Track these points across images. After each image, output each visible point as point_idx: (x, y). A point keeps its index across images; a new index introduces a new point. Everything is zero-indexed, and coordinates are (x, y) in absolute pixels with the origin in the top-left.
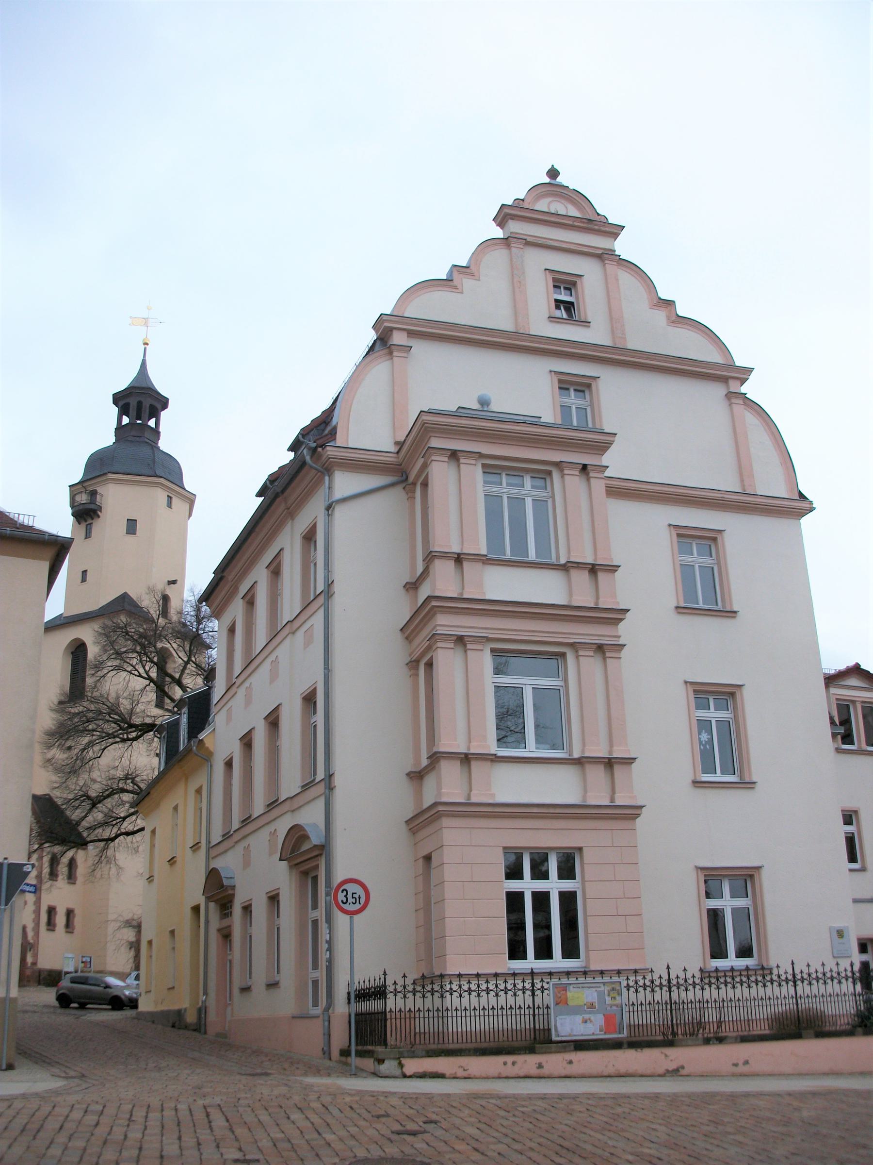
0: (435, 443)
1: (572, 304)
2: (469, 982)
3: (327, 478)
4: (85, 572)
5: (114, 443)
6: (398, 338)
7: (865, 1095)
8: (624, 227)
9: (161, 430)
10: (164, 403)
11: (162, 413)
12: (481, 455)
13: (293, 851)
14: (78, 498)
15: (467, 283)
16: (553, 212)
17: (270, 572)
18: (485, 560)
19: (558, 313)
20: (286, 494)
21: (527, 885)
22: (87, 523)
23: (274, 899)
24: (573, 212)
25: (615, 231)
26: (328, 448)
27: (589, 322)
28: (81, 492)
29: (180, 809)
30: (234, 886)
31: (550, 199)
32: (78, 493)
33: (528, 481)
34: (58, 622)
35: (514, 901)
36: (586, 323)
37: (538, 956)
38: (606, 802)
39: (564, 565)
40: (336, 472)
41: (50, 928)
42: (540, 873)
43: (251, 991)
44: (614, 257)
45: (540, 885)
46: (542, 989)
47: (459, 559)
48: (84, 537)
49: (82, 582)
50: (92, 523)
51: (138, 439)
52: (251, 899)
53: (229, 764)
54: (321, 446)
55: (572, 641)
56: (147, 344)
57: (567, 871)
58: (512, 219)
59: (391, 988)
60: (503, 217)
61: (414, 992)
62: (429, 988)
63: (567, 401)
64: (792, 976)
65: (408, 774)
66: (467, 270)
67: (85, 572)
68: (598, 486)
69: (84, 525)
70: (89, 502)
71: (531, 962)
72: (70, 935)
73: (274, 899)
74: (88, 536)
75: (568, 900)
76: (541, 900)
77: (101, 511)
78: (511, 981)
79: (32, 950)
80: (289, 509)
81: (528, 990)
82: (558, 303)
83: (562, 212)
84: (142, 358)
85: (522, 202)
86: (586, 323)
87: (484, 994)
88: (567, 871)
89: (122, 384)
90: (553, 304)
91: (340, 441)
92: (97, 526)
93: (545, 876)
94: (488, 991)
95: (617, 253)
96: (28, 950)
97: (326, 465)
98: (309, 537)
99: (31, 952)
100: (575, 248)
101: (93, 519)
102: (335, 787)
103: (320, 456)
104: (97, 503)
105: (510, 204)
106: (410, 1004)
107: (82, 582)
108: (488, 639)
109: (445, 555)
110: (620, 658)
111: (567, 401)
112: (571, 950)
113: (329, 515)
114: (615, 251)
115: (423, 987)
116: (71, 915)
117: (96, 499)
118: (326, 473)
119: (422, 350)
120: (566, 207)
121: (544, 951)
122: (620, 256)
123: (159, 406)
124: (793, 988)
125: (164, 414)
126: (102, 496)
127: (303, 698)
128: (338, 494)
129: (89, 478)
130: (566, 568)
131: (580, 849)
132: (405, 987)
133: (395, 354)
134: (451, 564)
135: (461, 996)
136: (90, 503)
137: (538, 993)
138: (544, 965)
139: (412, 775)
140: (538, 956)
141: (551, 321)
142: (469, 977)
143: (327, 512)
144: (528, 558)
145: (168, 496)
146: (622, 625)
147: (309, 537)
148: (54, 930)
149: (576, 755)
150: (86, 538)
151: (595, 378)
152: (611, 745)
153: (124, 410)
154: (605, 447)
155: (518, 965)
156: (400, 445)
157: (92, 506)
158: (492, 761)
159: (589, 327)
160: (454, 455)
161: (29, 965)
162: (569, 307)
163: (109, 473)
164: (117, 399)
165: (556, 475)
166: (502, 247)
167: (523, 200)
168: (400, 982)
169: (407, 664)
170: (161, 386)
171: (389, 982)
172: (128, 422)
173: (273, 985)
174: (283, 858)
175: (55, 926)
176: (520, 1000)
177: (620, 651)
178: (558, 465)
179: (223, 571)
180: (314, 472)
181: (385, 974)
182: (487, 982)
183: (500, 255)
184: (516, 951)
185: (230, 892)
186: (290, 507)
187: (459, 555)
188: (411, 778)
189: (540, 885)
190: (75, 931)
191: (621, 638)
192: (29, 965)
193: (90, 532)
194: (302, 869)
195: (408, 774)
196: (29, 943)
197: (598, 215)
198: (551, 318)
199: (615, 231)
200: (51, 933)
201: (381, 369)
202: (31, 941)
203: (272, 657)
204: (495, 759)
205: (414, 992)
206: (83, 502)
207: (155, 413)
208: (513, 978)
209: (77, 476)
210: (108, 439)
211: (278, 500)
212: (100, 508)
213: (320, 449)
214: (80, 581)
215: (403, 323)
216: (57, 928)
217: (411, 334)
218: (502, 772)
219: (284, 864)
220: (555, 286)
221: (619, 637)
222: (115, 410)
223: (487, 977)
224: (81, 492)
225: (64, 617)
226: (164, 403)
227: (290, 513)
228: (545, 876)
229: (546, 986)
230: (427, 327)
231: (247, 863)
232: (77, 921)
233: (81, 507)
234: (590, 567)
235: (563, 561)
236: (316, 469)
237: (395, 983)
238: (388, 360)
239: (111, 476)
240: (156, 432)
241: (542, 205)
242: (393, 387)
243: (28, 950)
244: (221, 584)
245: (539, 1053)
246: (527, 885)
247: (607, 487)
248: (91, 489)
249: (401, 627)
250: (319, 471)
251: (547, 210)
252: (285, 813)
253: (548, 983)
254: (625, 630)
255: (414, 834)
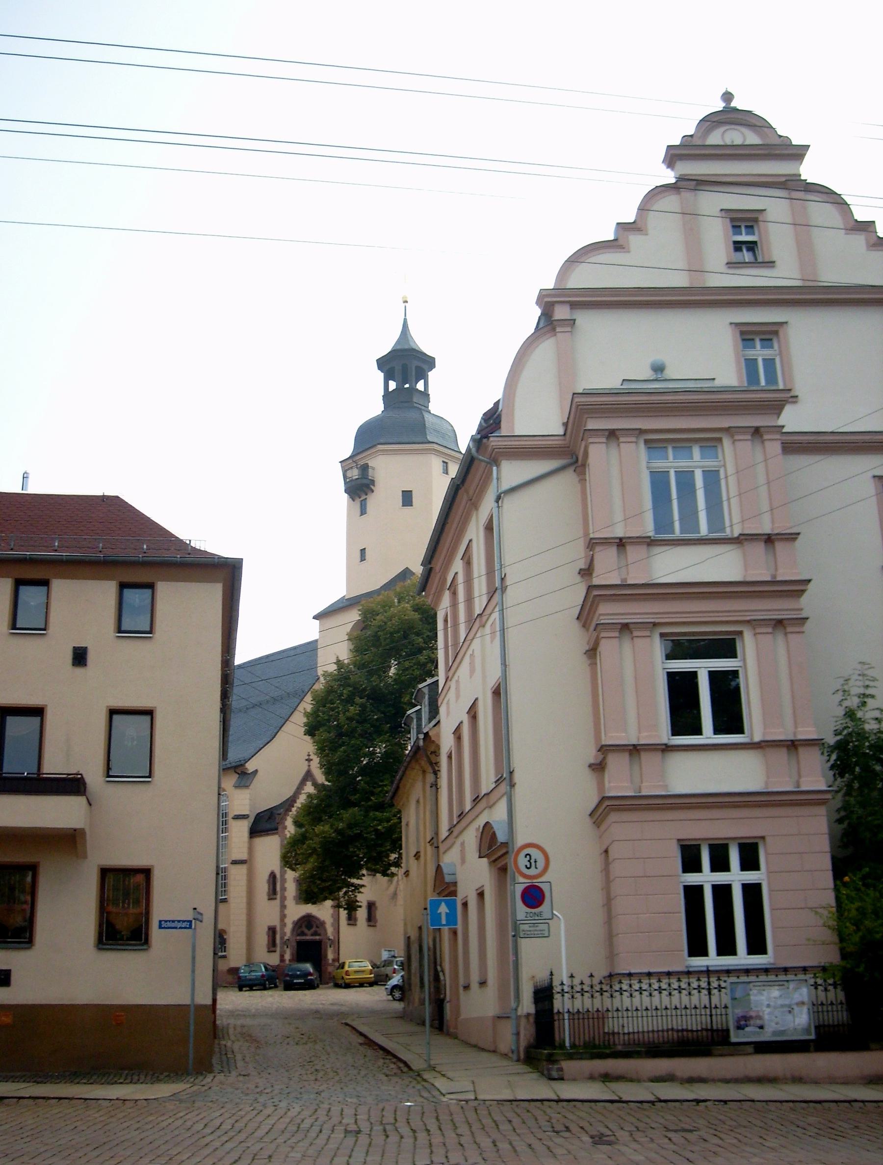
0: (592, 424)
1: (755, 243)
2: (640, 982)
3: (495, 468)
4: (363, 551)
5: (382, 412)
6: (561, 313)
7: (6, 1079)
8: (809, 146)
9: (431, 391)
10: (430, 363)
11: (429, 373)
12: (641, 432)
13: (490, 847)
14: (349, 474)
15: (634, 240)
16: (729, 144)
17: (463, 563)
18: (651, 542)
19: (737, 257)
20: (466, 484)
21: (707, 878)
22: (361, 499)
23: (481, 895)
24: (752, 138)
25: (798, 153)
26: (491, 439)
27: (774, 262)
28: (352, 468)
29: (421, 801)
30: (456, 883)
31: (722, 129)
32: (348, 469)
33: (696, 452)
34: (341, 605)
35: (693, 894)
36: (770, 264)
37: (720, 952)
38: (790, 788)
39: (737, 538)
40: (502, 461)
41: (351, 922)
42: (720, 864)
43: (470, 989)
44: (799, 183)
45: (721, 878)
46: (720, 988)
47: (621, 543)
48: (359, 513)
49: (362, 560)
50: (366, 499)
51: (406, 405)
52: (467, 897)
53: (450, 757)
54: (485, 438)
55: (748, 618)
56: (407, 302)
57: (750, 862)
58: (681, 160)
59: (557, 989)
60: (673, 156)
61: (602, 991)
62: (617, 987)
63: (751, 353)
64: (706, 984)
65: (590, 766)
66: (633, 226)
67: (363, 551)
68: (774, 448)
69: (358, 501)
70: (360, 477)
71: (713, 960)
72: (372, 928)
73: (481, 895)
74: (363, 513)
75: (752, 892)
76: (722, 893)
77: (374, 486)
78: (645, 981)
79: (332, 946)
80: (471, 500)
81: (703, 989)
82: (738, 246)
83: (738, 141)
84: (404, 317)
85: (690, 138)
86: (770, 264)
87: (656, 993)
88: (750, 862)
89: (385, 349)
90: (731, 246)
91: (504, 431)
92: (373, 501)
93: (726, 868)
94: (660, 990)
95: (802, 178)
96: (329, 946)
97: (493, 455)
98: (489, 528)
99: (332, 948)
100: (758, 180)
101: (366, 495)
102: (515, 784)
103: (487, 447)
104: (370, 478)
105: (678, 143)
106: (597, 1003)
107: (362, 560)
108: (655, 625)
109: (605, 542)
110: (803, 632)
111: (751, 353)
112: (757, 945)
113: (498, 507)
114: (800, 175)
115: (611, 987)
116: (373, 908)
117: (368, 472)
118: (493, 463)
119: (587, 321)
120: (743, 134)
121: (726, 947)
122: (806, 180)
123: (425, 367)
124: (707, 997)
125: (431, 375)
126: (373, 469)
127: (493, 692)
128: (505, 485)
129: (359, 451)
130: (740, 540)
131: (763, 838)
132: (592, 987)
133: (558, 329)
134: (613, 551)
135: (592, 996)
136: (361, 478)
137: (715, 992)
138: (727, 961)
139: (594, 767)
140: (720, 952)
141: (729, 267)
142: (640, 976)
143: (496, 505)
144: (699, 533)
145: (443, 462)
146: (806, 595)
147: (489, 528)
148: (356, 925)
149: (757, 738)
150: (362, 514)
151: (781, 324)
152: (796, 726)
153: (389, 376)
154: (781, 405)
155: (699, 962)
156: (566, 425)
157: (365, 481)
158: (663, 751)
159: (773, 267)
160: (612, 434)
161: (330, 961)
162: (752, 246)
163: (378, 444)
164: (384, 364)
165: (727, 442)
166: (667, 194)
167: (691, 136)
168: (587, 981)
169: (585, 653)
170: (424, 343)
171: (556, 983)
172: (395, 387)
173: (483, 983)
174: (482, 855)
175: (356, 920)
176: (695, 999)
177: (803, 624)
178: (727, 430)
179: (430, 563)
180: (483, 464)
181: (552, 974)
182: (659, 981)
183: (671, 202)
184: (697, 947)
185: (452, 889)
186: (473, 497)
187: (621, 539)
188: (593, 770)
189: (721, 878)
190: (378, 924)
191: (803, 611)
192: (330, 961)
193: (365, 509)
194: (500, 865)
195: (590, 766)
196: (329, 939)
197: (780, 136)
198: (730, 264)
199: (798, 153)
200: (351, 928)
201: (547, 347)
202: (331, 937)
203: (470, 652)
204: (667, 749)
205: (602, 991)
206: (354, 478)
207: (422, 375)
208: (628, 978)
209: (347, 449)
210: (376, 408)
211: (460, 492)
212: (373, 482)
213: (485, 440)
214: (360, 560)
215: (565, 296)
216: (358, 923)
217: (574, 305)
218: (677, 761)
219: (485, 860)
220: (734, 227)
221: (802, 609)
222: (381, 376)
223: (660, 976)
224: (352, 468)
225: (346, 600)
226: (430, 363)
227: (473, 504)
228: (726, 868)
229: (723, 985)
230: (592, 296)
231: (463, 861)
232: (379, 914)
233: (353, 483)
234: (766, 537)
235: (736, 535)
236: (484, 461)
237: (582, 983)
238: (551, 337)
239: (380, 447)
240: (425, 395)
241: (715, 138)
242: (47, 612)
243: (329, 946)
244: (432, 575)
245: (716, 1056)
246: (707, 878)
247: (782, 443)
248: (361, 463)
249: (577, 616)
250: (488, 463)
251: (721, 143)
252: (483, 811)
253: (725, 981)
254: (807, 603)
255: (598, 827)
